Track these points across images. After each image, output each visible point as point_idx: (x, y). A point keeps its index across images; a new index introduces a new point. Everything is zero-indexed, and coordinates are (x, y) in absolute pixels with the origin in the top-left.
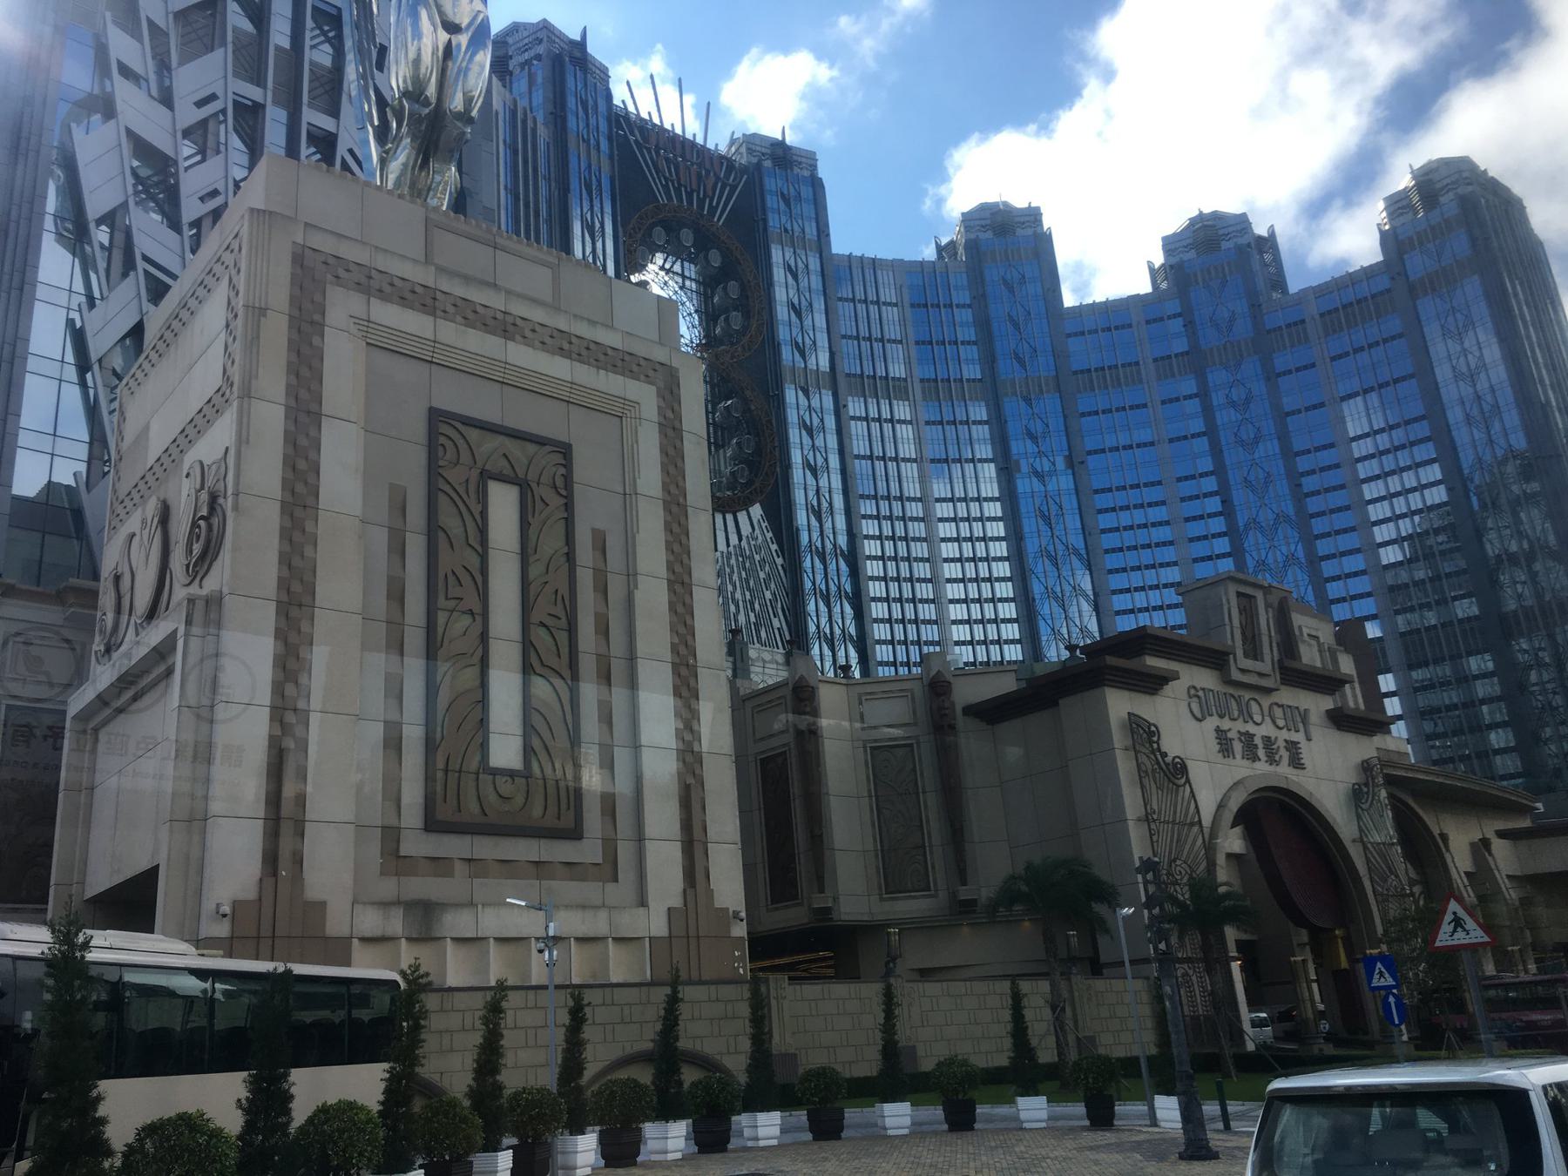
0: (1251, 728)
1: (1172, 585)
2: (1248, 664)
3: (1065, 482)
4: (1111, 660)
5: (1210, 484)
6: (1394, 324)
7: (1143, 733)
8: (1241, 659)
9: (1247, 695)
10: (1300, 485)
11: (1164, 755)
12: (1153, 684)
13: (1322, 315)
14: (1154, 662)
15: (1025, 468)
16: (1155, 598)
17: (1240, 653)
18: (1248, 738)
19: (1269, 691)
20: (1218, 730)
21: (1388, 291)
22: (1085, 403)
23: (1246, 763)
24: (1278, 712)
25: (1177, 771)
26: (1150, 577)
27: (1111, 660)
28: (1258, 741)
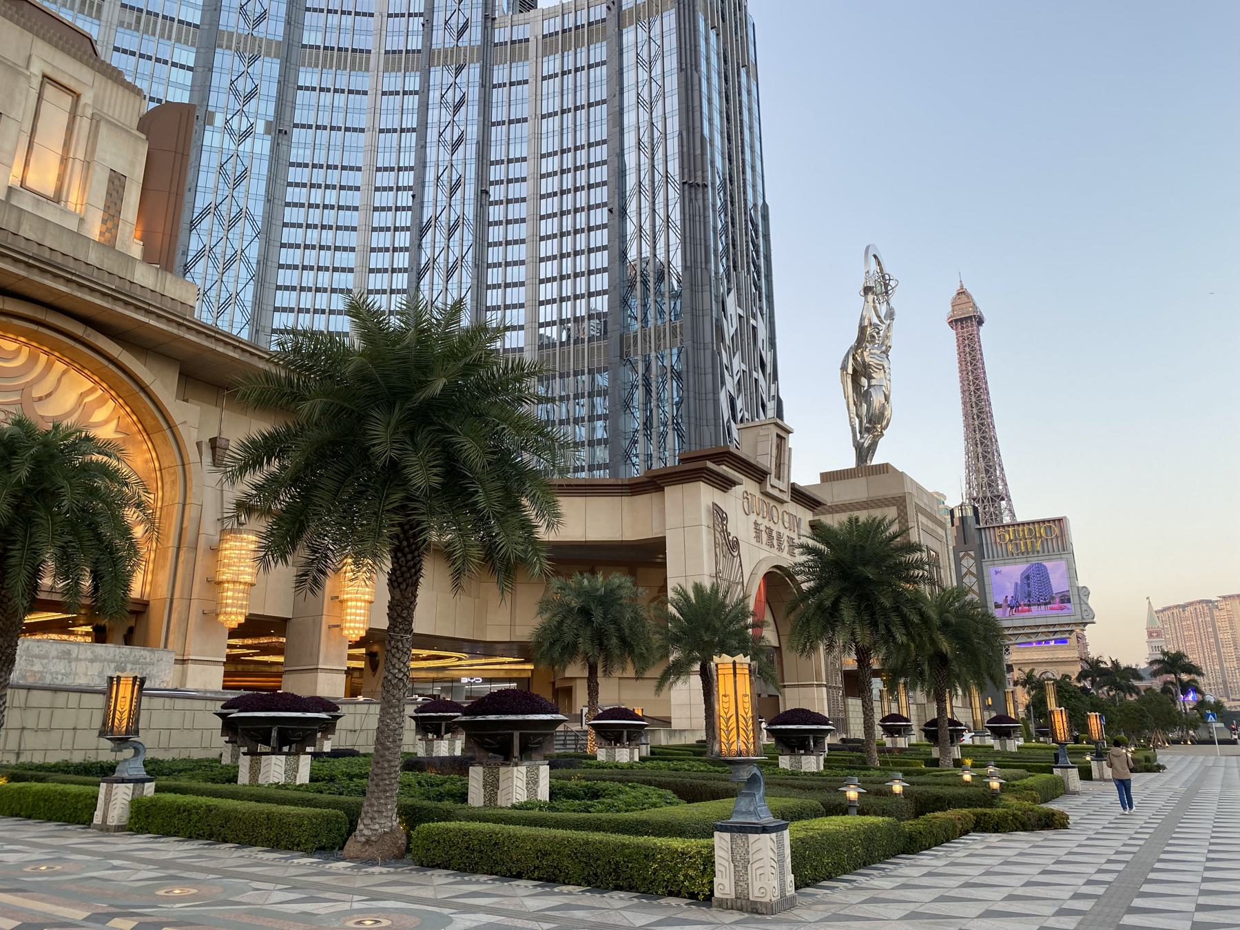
0: (771, 525)
1: (342, 291)
2: (775, 482)
3: (261, 145)
4: (710, 465)
5: (407, 179)
6: (600, 52)
7: (719, 515)
8: (772, 479)
9: (772, 503)
10: (487, 193)
11: (729, 534)
12: (725, 484)
13: (544, 37)
14: (724, 469)
15: (219, 120)
16: (322, 301)
17: (773, 476)
18: (769, 531)
19: (782, 502)
20: (756, 523)
21: (604, 20)
22: (307, 77)
23: (768, 548)
24: (786, 517)
25: (734, 545)
26: (324, 279)
27: (710, 465)
28: (774, 534)
